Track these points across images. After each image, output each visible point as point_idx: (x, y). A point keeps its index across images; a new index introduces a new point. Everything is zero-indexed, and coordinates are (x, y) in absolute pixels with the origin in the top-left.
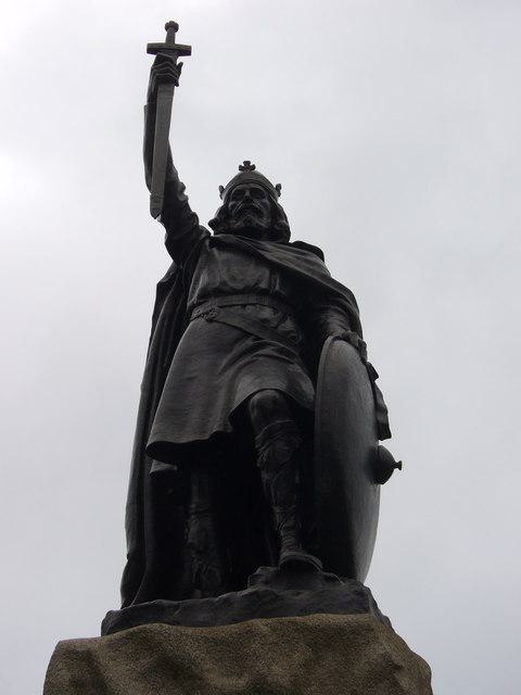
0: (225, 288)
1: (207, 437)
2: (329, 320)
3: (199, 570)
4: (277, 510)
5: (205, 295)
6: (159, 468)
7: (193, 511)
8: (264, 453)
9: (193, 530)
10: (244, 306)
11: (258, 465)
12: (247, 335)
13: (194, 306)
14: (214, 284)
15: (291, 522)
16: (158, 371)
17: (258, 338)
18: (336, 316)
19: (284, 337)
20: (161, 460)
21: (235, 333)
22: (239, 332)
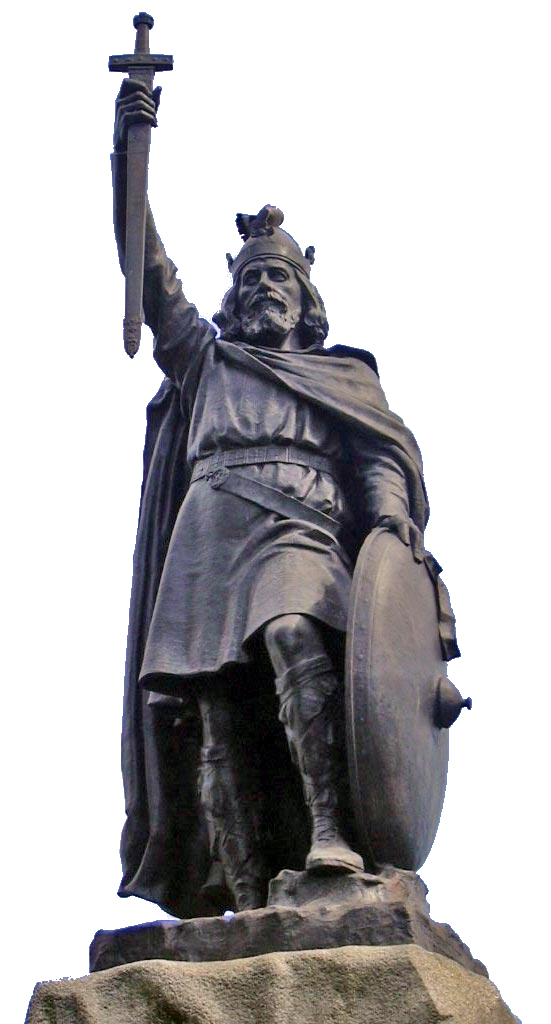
0: (233, 437)
1: (193, 306)
2: (375, 480)
3: (217, 840)
4: (307, 780)
5: (208, 446)
6: (157, 700)
7: (206, 759)
8: (287, 703)
9: (207, 781)
10: (261, 465)
11: (280, 717)
12: (267, 512)
13: (195, 459)
14: (398, 802)
15: (325, 798)
16: (155, 540)
17: (282, 518)
18: (387, 472)
19: (319, 512)
20: (158, 690)
21: (254, 511)
22: (299, 616)
